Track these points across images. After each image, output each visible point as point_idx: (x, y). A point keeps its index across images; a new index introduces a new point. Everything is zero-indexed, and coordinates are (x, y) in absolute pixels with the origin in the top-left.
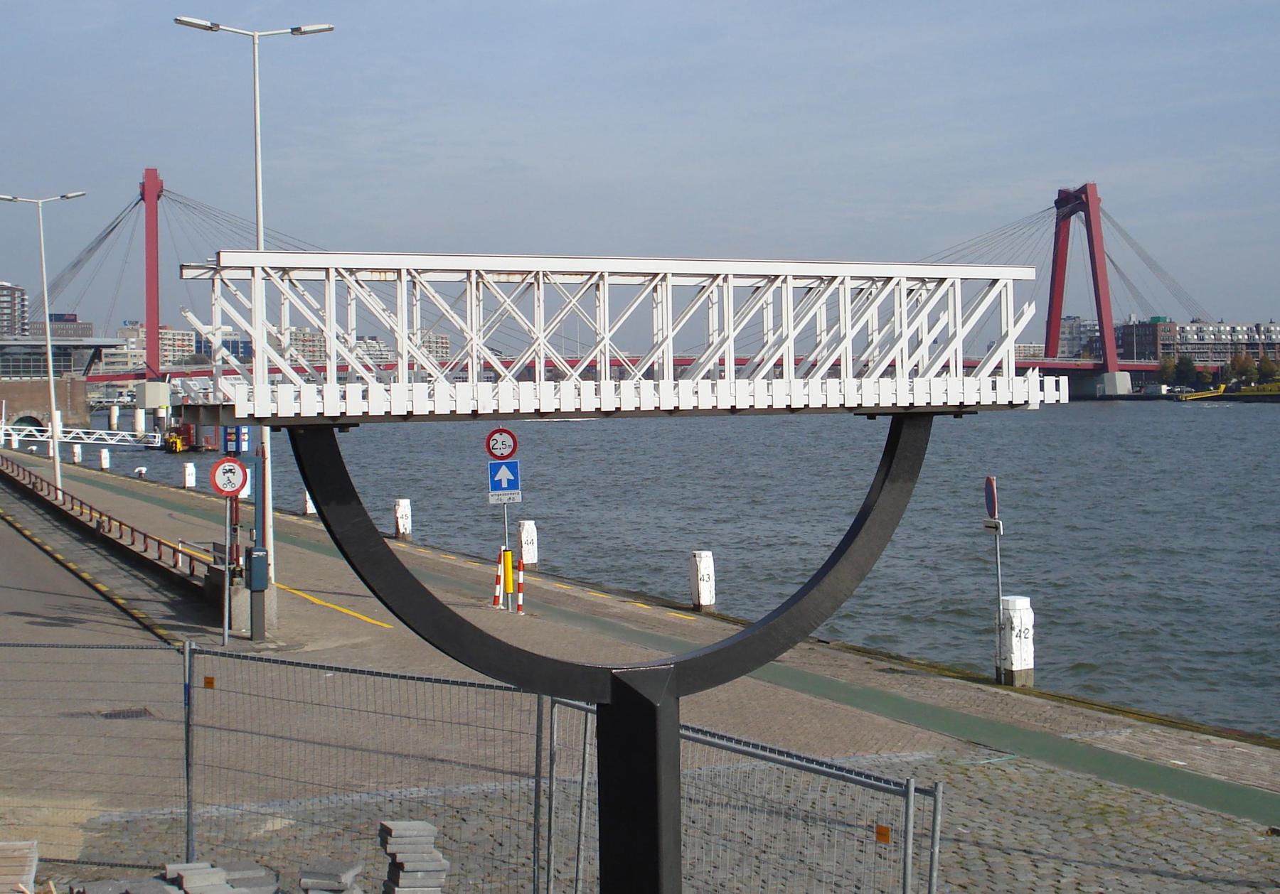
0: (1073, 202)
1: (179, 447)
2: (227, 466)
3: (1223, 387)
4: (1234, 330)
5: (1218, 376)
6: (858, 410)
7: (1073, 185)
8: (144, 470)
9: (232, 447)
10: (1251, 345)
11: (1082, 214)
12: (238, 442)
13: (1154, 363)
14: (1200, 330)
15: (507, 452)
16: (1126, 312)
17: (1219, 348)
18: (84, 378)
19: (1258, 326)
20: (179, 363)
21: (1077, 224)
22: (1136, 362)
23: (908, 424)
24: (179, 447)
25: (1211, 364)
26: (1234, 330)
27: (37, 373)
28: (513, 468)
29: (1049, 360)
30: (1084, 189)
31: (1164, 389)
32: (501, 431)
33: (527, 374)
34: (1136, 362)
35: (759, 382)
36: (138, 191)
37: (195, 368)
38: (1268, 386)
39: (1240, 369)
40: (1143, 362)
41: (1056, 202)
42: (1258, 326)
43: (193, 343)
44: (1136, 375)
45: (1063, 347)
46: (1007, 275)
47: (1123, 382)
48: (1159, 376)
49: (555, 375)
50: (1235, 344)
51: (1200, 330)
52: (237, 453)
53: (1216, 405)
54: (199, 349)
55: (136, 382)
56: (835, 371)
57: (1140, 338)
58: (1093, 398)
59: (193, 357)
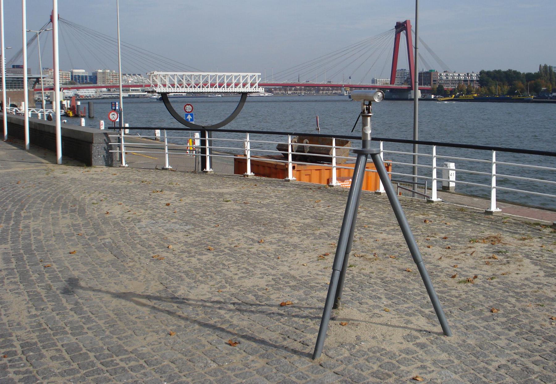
0: (401, 27)
1: (71, 115)
2: (113, 113)
3: (454, 96)
4: (459, 75)
5: (452, 92)
6: (237, 92)
7: (402, 20)
8: (66, 121)
9: (114, 108)
10: (465, 81)
11: (405, 31)
12: (115, 106)
13: (430, 87)
14: (447, 75)
15: (190, 111)
16: (421, 68)
17: (453, 81)
18: (33, 90)
19: (468, 74)
20: (66, 84)
21: (403, 35)
22: (423, 86)
23: (244, 94)
24: (71, 115)
25: (450, 88)
26: (459, 75)
27: (19, 88)
28: (192, 115)
29: (391, 85)
30: (405, 22)
31: (433, 96)
32: (188, 105)
33: (191, 87)
34: (423, 86)
35: (213, 88)
36: (49, 18)
37: (72, 86)
38: (469, 96)
39: (460, 90)
40: (426, 87)
41: (395, 27)
42: (468, 74)
43: (70, 76)
44: (423, 91)
45: (397, 81)
46: (257, 74)
47: (419, 94)
48: (431, 92)
49: (195, 87)
50: (459, 80)
51: (447, 75)
52: (115, 110)
53: (450, 102)
54: (72, 79)
55: (49, 91)
56: (224, 87)
57: (427, 77)
58: (407, 99)
59: (70, 82)
